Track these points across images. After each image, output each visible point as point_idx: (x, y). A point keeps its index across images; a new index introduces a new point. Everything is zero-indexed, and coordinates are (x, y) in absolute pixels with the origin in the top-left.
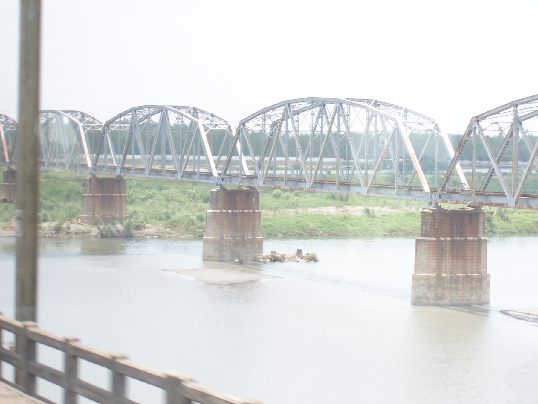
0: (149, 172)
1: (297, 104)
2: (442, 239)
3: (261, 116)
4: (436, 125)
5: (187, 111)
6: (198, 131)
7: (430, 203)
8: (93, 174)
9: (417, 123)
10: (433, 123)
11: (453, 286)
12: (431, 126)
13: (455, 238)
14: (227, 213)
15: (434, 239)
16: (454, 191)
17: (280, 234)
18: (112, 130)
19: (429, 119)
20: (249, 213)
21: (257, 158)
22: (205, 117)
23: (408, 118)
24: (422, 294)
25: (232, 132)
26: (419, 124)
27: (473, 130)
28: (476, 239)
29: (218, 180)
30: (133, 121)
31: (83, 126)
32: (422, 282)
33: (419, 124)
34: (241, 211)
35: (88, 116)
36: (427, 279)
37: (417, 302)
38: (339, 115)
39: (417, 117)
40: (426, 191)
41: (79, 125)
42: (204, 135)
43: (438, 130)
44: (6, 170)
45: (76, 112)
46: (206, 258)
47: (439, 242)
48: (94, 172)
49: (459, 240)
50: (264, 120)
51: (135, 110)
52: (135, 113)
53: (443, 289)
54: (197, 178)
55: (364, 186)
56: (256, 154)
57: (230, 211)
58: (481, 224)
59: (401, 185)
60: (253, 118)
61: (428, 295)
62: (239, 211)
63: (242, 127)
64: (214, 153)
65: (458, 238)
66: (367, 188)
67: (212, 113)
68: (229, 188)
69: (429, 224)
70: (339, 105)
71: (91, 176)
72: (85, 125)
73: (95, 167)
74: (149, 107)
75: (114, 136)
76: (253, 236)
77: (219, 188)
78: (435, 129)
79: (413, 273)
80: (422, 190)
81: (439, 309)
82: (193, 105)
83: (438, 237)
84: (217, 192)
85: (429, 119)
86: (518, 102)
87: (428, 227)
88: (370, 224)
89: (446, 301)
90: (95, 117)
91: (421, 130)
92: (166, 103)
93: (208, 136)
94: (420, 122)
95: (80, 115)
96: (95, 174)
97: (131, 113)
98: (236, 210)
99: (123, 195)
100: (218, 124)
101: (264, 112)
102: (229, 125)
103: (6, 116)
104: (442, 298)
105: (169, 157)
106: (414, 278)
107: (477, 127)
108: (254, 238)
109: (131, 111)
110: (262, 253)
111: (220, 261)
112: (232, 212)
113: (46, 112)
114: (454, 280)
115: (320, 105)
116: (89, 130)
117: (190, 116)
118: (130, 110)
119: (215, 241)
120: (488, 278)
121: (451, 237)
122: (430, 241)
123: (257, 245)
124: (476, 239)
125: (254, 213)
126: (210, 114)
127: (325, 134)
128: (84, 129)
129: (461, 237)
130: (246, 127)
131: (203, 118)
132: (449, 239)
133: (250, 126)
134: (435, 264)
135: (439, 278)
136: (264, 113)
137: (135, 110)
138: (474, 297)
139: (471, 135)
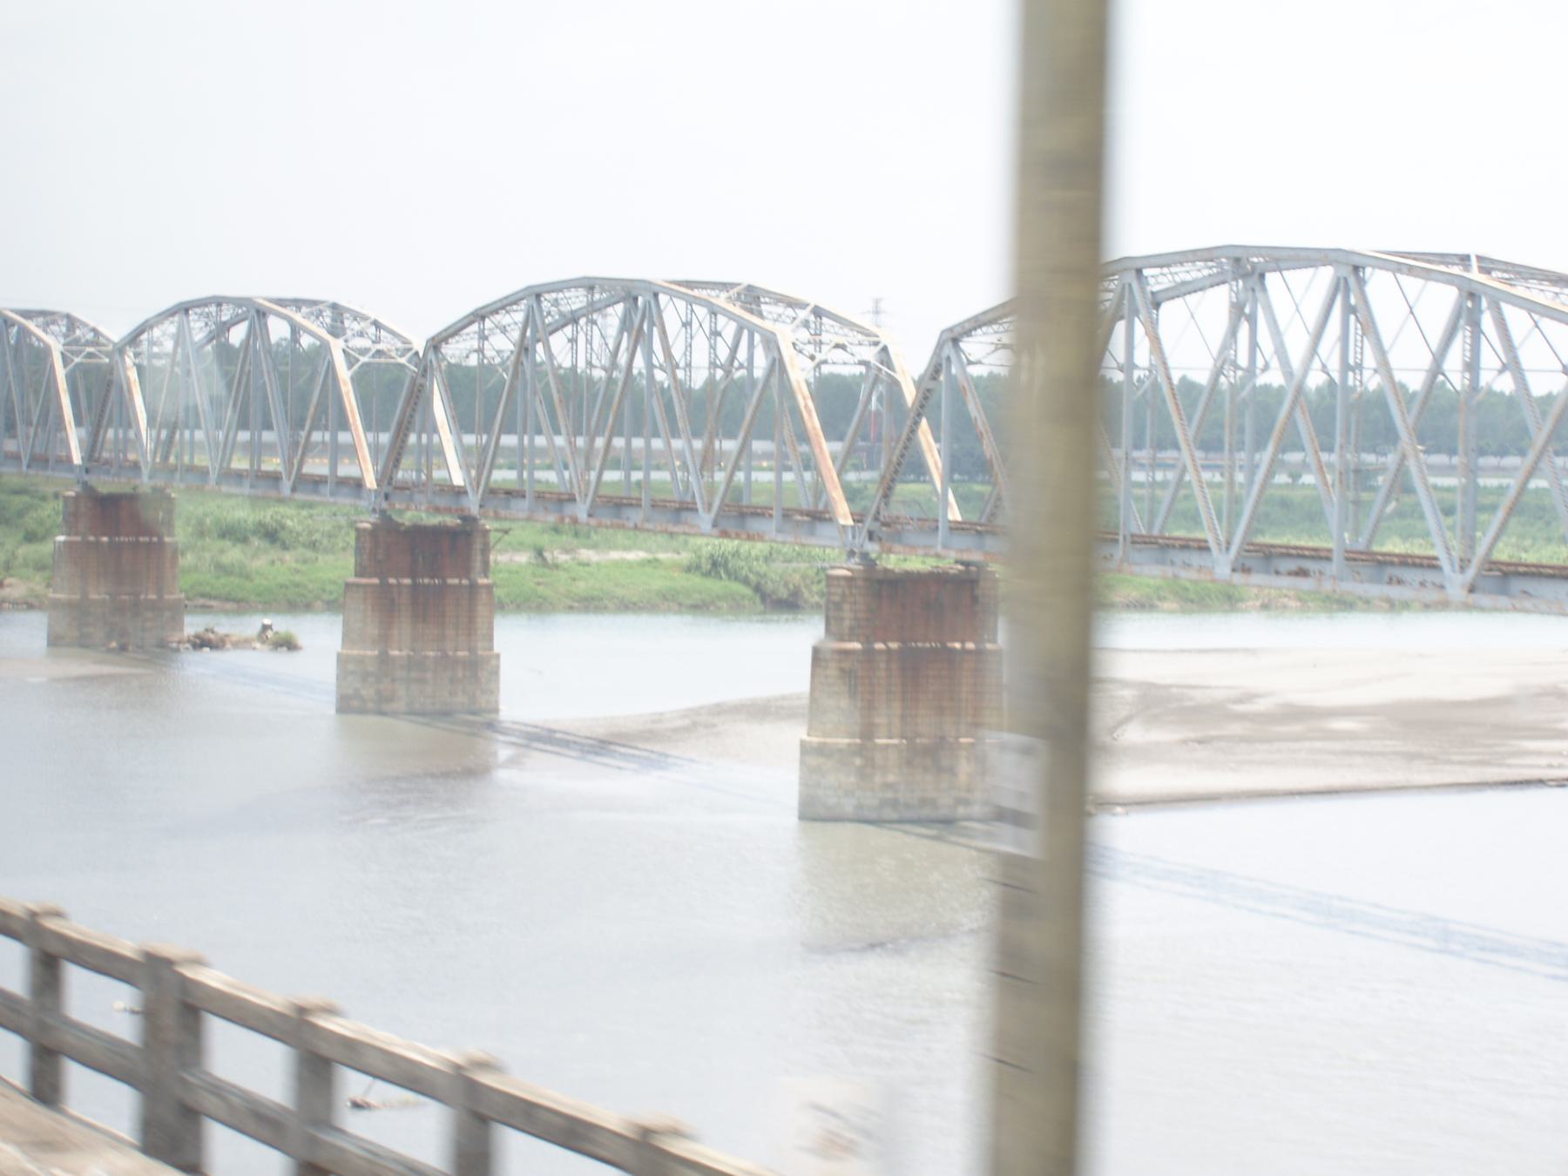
0: (482, 499)
1: (1165, 270)
2: (392, 581)
3: (475, 327)
4: (885, 349)
5: (730, 298)
6: (331, 367)
7: (851, 554)
8: (383, 512)
9: (833, 344)
10: (876, 344)
11: (414, 674)
12: (870, 354)
13: (421, 581)
14: (98, 544)
15: (376, 581)
16: (405, 485)
17: (319, 603)
18: (449, 363)
19: (868, 335)
20: (150, 543)
21: (698, 444)
22: (794, 319)
23: (823, 333)
24: (350, 691)
25: (894, 371)
26: (837, 346)
27: (944, 363)
28: (465, 582)
29: (854, 537)
30: (528, 333)
31: (62, 353)
32: (351, 667)
33: (837, 346)
34: (933, 645)
35: (357, 317)
36: (360, 660)
37: (346, 705)
38: (1349, 310)
39: (846, 330)
40: (842, 522)
41: (332, 345)
42: (344, 374)
43: (890, 365)
44: (368, 526)
45: (314, 303)
46: (54, 641)
47: (384, 588)
48: (385, 505)
49: (428, 586)
50: (483, 337)
51: (537, 294)
52: (535, 306)
53: (393, 680)
54: (328, 494)
55: (1220, 550)
56: (696, 434)
57: (105, 539)
58: (478, 552)
59: (1137, 532)
60: (453, 335)
61: (364, 692)
62: (127, 539)
63: (948, 350)
64: (368, 427)
65: (426, 581)
66: (712, 515)
67: (816, 307)
68: (103, 489)
69: (367, 551)
70: (1346, 272)
71: (374, 518)
72: (68, 351)
73: (386, 489)
74: (589, 285)
75: (462, 384)
76: (160, 592)
77: (856, 564)
78: (882, 363)
79: (339, 650)
80: (830, 520)
81: (386, 720)
82: (745, 279)
83: (382, 575)
84: (77, 498)
85: (868, 335)
86: (483, 311)
87: (365, 557)
88: (539, 584)
89: (400, 705)
90: (382, 320)
91: (844, 366)
92: (260, 290)
93: (357, 380)
94: (841, 340)
95: (328, 313)
96: (389, 513)
97: (523, 305)
98: (119, 537)
99: (454, 581)
100: (846, 344)
101: (480, 316)
102: (881, 346)
103: (68, 317)
104: (390, 699)
105: (268, 436)
106: (342, 660)
107: (953, 358)
108: (160, 597)
109: (522, 299)
110: (182, 630)
111: (815, 820)
112: (111, 542)
113: (211, 303)
114: (413, 664)
115: (623, 300)
116: (364, 365)
117: (737, 310)
118: (521, 295)
119: (70, 605)
120: (494, 662)
121: (413, 576)
122: (365, 586)
123: (167, 614)
124: (465, 582)
125: (473, 587)
126: (369, 321)
127: (758, 379)
128: (66, 361)
129: (432, 577)
130: (441, 356)
131: (788, 321)
132: (407, 581)
133: (454, 351)
134: (376, 632)
135: (384, 659)
136: (483, 318)
137: (538, 296)
138: (461, 699)
139: (942, 378)
